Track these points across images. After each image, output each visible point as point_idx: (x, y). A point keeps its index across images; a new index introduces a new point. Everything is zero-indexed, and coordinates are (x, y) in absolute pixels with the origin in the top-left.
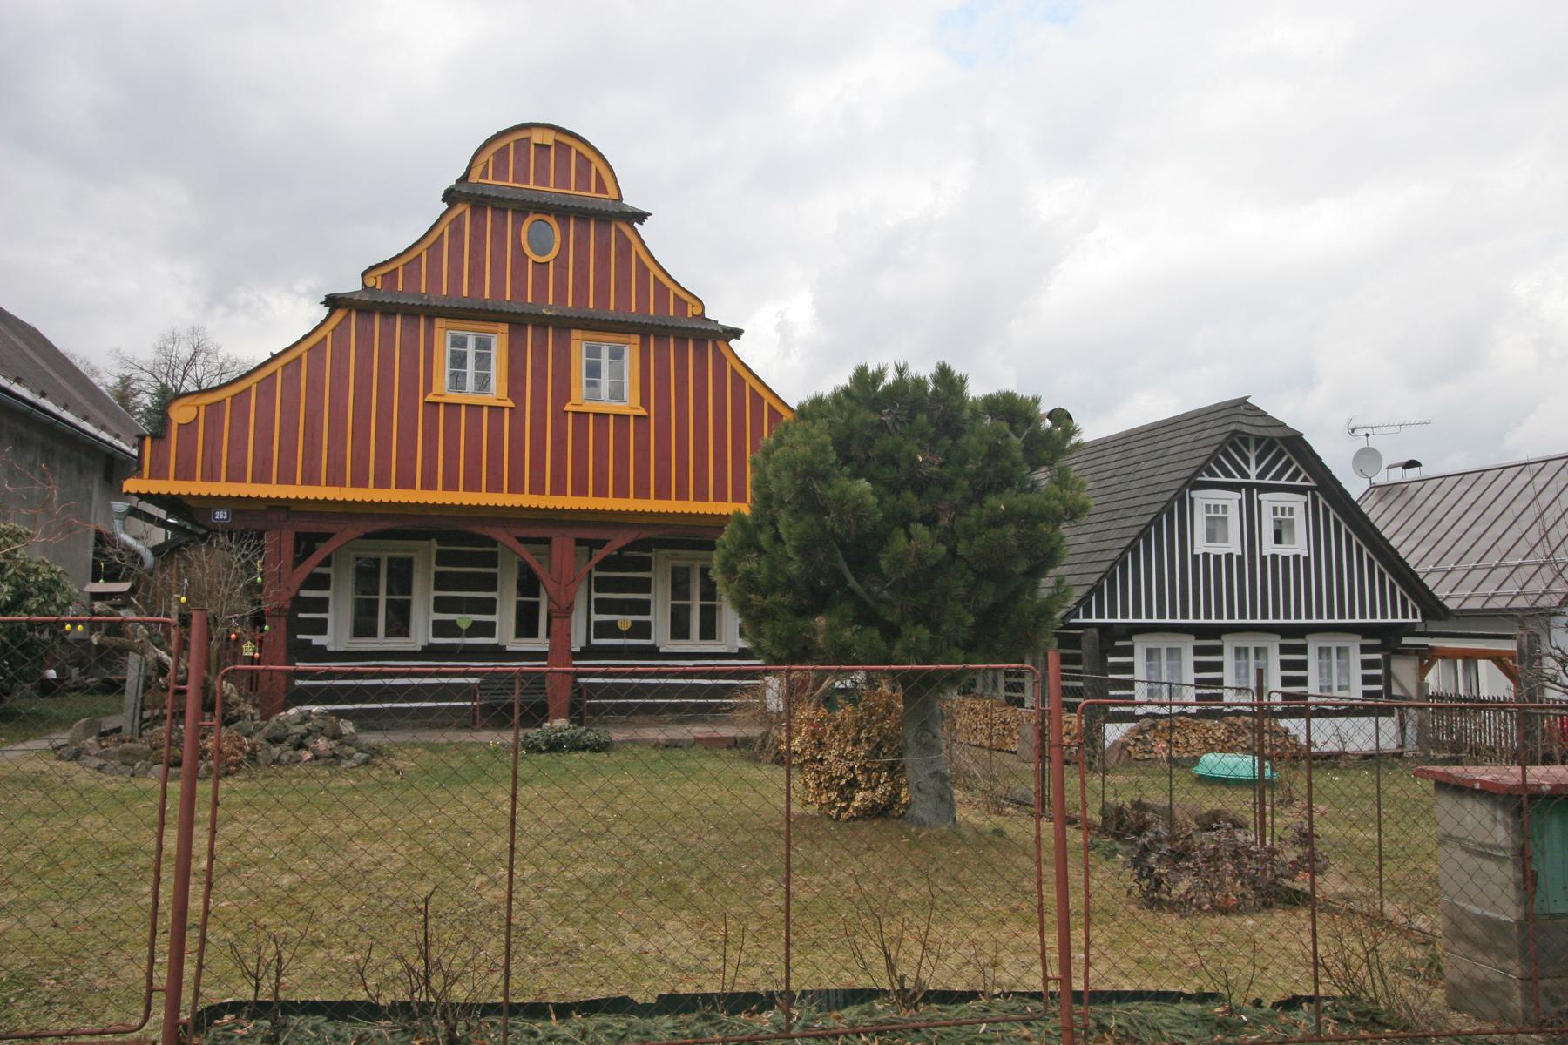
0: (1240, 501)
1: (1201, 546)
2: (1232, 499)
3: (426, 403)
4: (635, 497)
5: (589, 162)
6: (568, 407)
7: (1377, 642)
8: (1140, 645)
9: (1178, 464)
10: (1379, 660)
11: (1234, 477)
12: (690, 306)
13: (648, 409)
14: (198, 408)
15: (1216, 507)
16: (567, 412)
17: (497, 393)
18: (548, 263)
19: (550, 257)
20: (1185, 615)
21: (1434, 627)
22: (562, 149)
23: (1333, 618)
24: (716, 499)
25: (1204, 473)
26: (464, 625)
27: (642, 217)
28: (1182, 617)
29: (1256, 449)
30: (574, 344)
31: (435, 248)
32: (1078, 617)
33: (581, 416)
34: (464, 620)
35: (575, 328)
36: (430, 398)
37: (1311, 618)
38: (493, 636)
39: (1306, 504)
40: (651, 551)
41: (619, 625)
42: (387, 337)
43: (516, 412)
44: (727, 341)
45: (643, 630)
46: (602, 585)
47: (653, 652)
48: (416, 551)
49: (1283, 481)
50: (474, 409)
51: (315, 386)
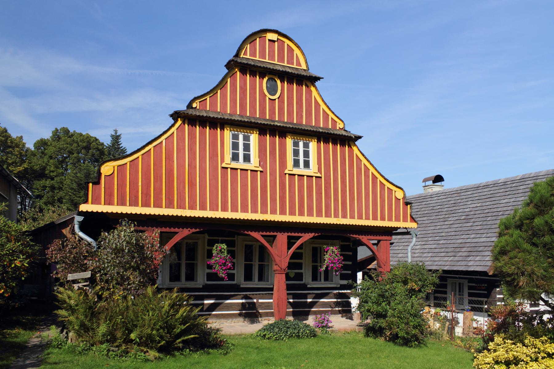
6: (286, 172)
12: (338, 124)
13: (321, 174)
14: (114, 167)
16: (286, 174)
18: (275, 100)
35: (288, 133)
36: (224, 165)
38: (234, 280)
42: (202, 135)
51: (169, 158)
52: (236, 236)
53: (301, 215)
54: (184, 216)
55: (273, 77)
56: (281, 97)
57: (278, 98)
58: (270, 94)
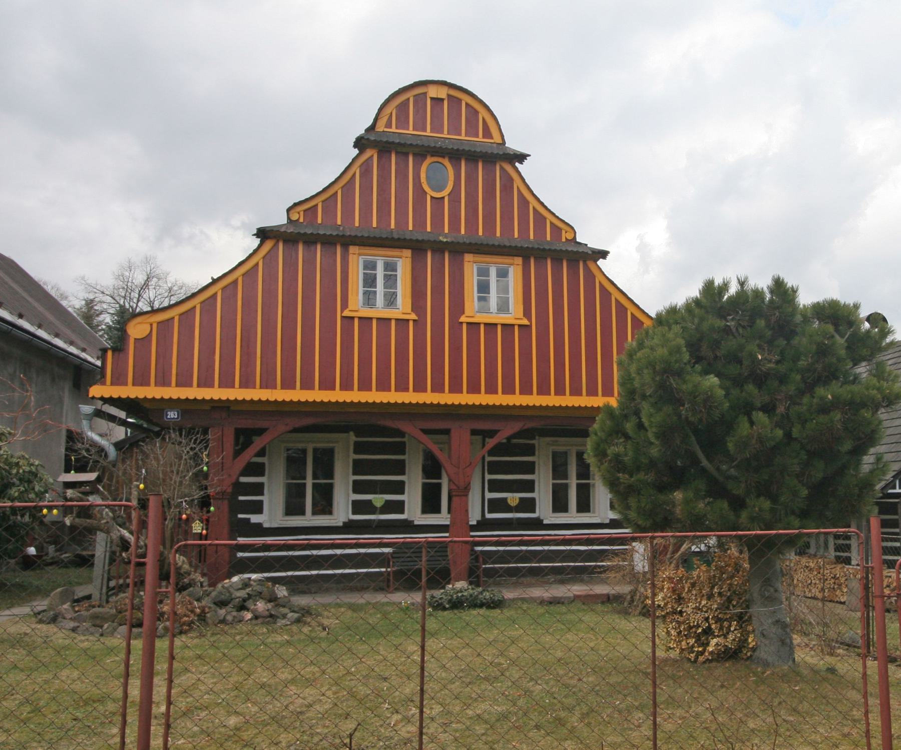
12: (563, 232)
13: (530, 319)
14: (151, 325)
16: (462, 323)
17: (403, 307)
18: (443, 198)
19: (445, 193)
34: (378, 500)
35: (351, 245)
36: (346, 313)
40: (534, 438)
41: (509, 501)
42: (309, 263)
43: (419, 324)
44: (596, 261)
45: (528, 505)
46: (494, 468)
47: (538, 524)
50: (384, 322)
52: (537, 437)
53: (491, 393)
54: (273, 399)
55: (440, 160)
56: (454, 195)
57: (449, 195)
58: (433, 189)
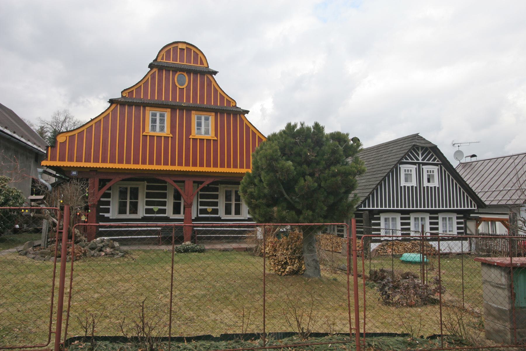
0: (416, 168)
1: (403, 183)
2: (413, 168)
3: (143, 135)
4: (213, 167)
5: (198, 55)
6: (191, 137)
7: (462, 216)
8: (383, 217)
9: (395, 156)
10: (463, 222)
11: (414, 160)
12: (231, 103)
13: (217, 138)
14: (66, 137)
15: (408, 170)
16: (190, 138)
17: (167, 132)
18: (184, 88)
19: (184, 86)
20: (397, 206)
21: (481, 210)
22: (189, 50)
23: (447, 208)
24: (240, 168)
25: (404, 159)
26: (156, 210)
27: (215, 73)
28: (397, 207)
29: (421, 151)
30: (193, 116)
31: (146, 83)
32: (361, 207)
33: (195, 140)
34: (156, 208)
35: (193, 110)
36: (144, 134)
37: (440, 208)
38: (165, 214)
39: (438, 169)
40: (218, 185)
41: (208, 210)
42: (130, 113)
43: (173, 138)
44: (244, 115)
45: (216, 212)
46: (202, 196)
47: (219, 219)
48: (139, 185)
49: (430, 162)
50: (159, 137)
51: (106, 130)
